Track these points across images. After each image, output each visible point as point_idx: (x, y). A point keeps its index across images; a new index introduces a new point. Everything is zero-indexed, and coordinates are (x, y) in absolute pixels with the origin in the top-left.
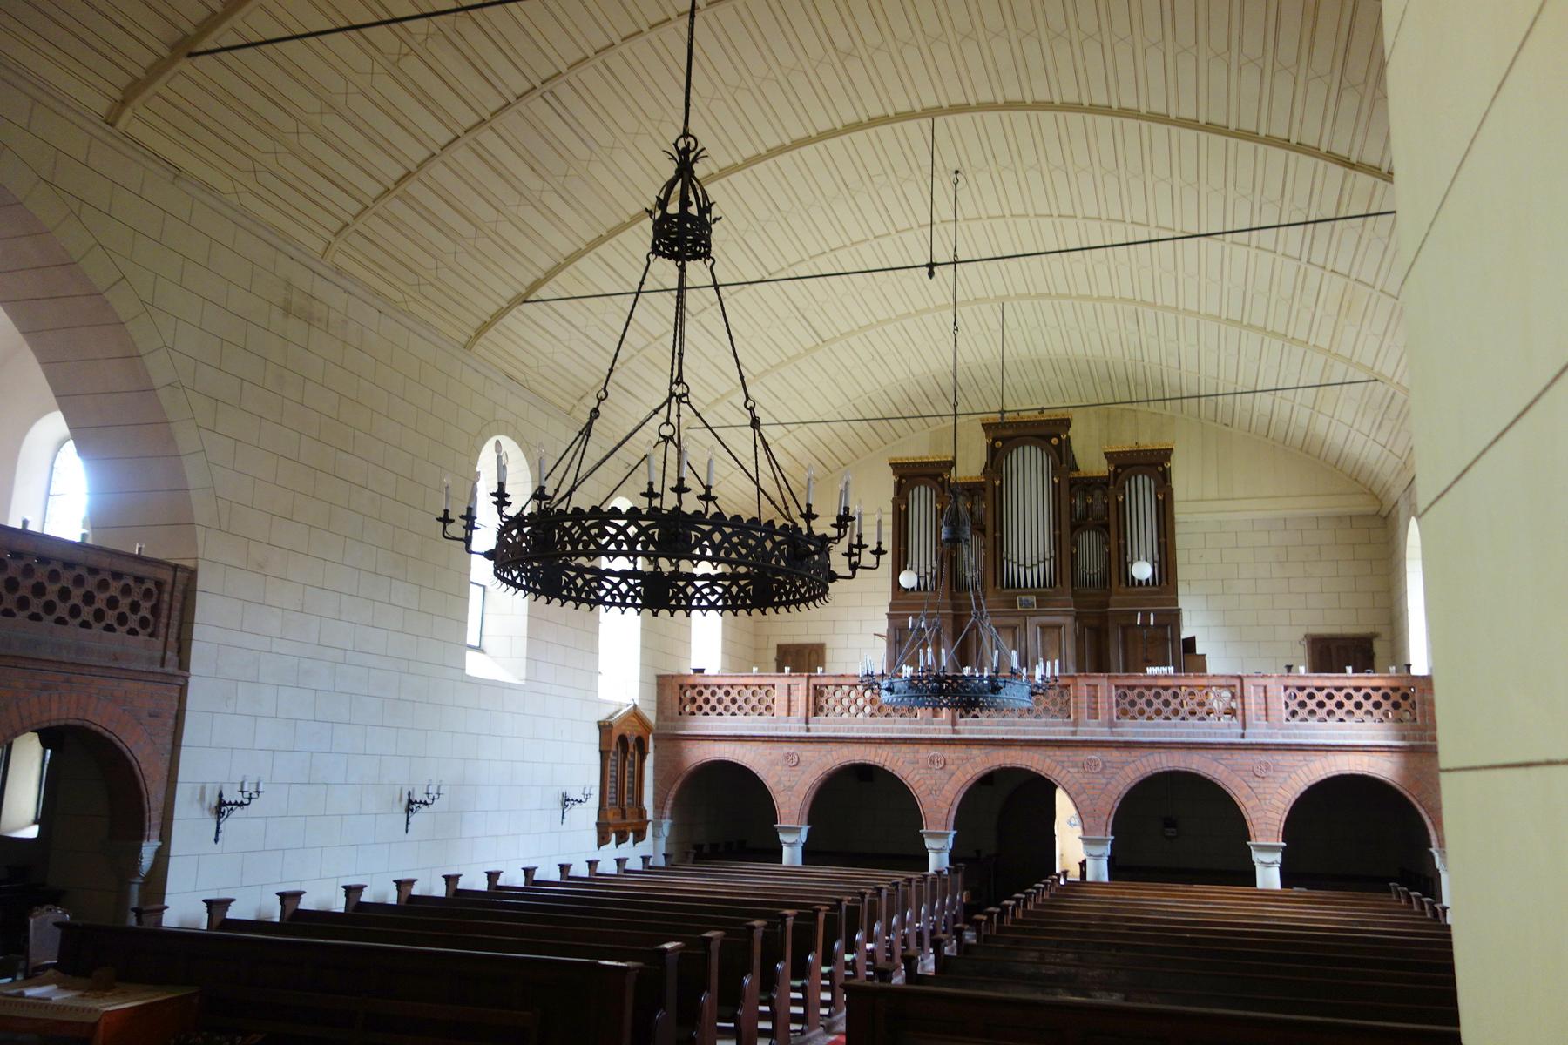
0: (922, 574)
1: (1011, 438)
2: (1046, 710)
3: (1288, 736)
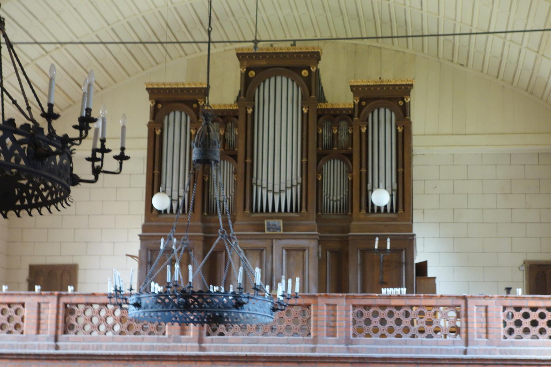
0: (175, 197)
1: (264, 68)
2: (288, 328)
3: (505, 352)
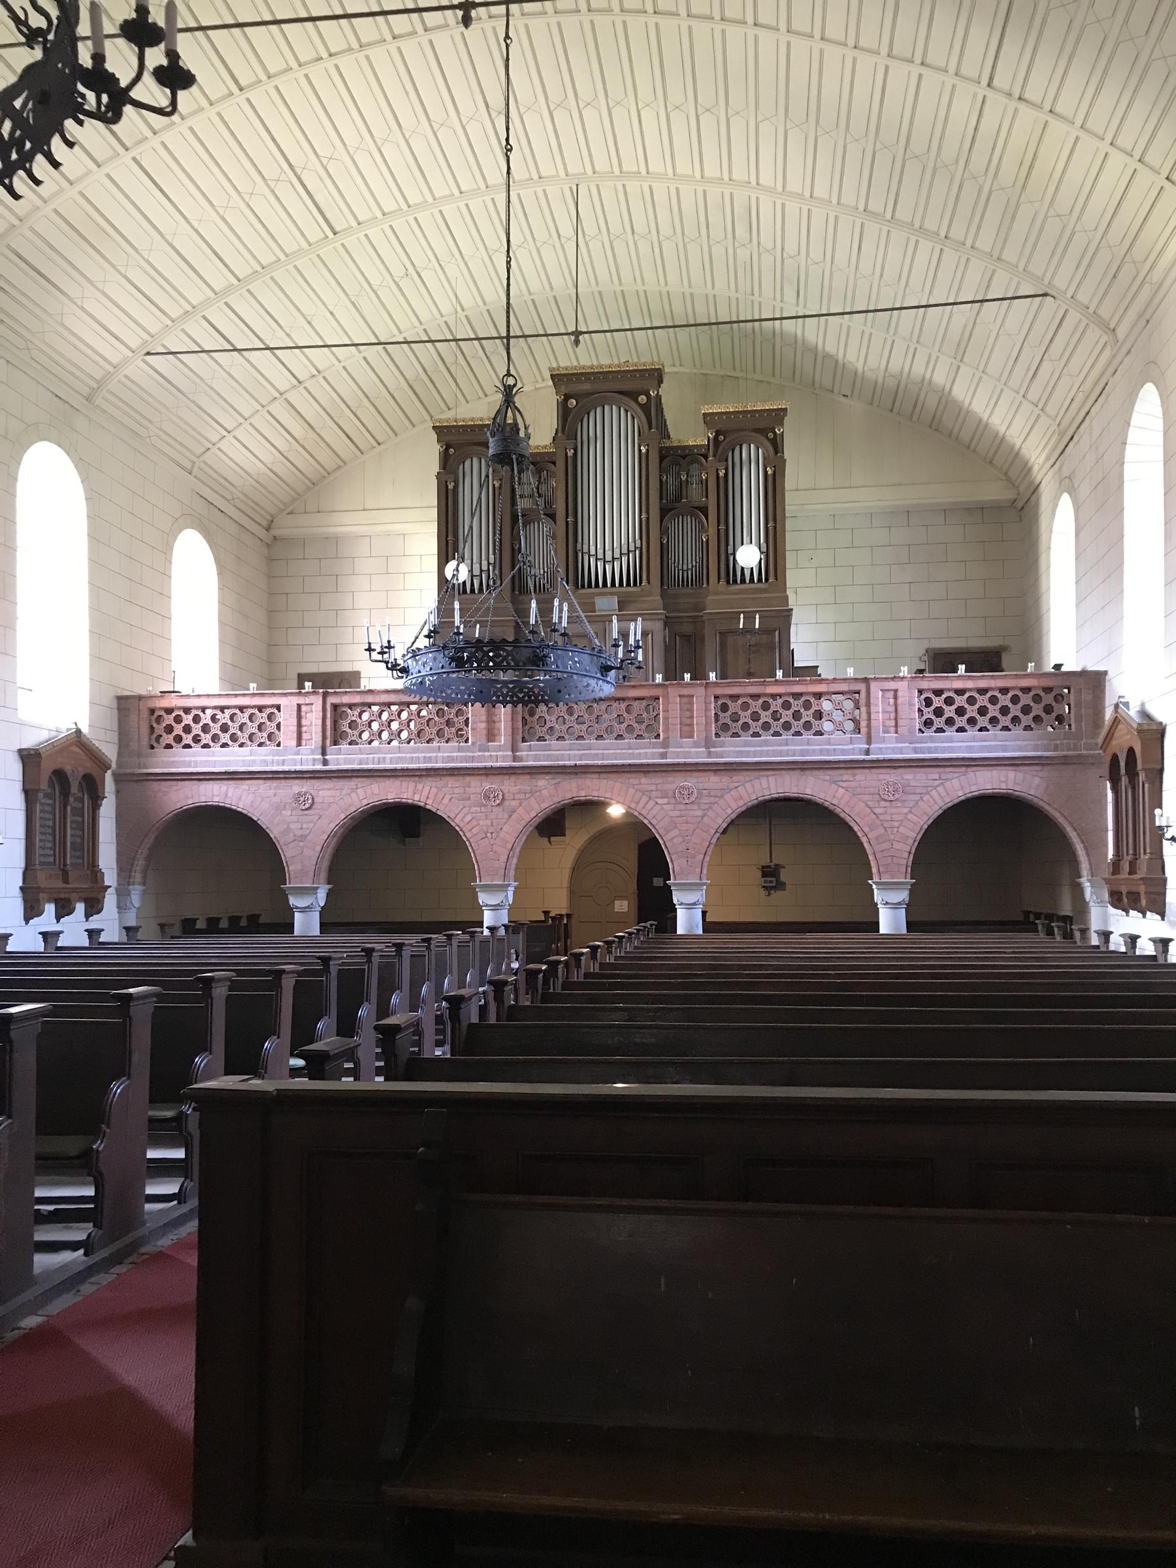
3: (921, 751)
